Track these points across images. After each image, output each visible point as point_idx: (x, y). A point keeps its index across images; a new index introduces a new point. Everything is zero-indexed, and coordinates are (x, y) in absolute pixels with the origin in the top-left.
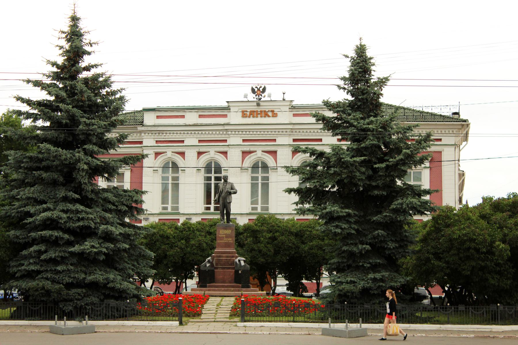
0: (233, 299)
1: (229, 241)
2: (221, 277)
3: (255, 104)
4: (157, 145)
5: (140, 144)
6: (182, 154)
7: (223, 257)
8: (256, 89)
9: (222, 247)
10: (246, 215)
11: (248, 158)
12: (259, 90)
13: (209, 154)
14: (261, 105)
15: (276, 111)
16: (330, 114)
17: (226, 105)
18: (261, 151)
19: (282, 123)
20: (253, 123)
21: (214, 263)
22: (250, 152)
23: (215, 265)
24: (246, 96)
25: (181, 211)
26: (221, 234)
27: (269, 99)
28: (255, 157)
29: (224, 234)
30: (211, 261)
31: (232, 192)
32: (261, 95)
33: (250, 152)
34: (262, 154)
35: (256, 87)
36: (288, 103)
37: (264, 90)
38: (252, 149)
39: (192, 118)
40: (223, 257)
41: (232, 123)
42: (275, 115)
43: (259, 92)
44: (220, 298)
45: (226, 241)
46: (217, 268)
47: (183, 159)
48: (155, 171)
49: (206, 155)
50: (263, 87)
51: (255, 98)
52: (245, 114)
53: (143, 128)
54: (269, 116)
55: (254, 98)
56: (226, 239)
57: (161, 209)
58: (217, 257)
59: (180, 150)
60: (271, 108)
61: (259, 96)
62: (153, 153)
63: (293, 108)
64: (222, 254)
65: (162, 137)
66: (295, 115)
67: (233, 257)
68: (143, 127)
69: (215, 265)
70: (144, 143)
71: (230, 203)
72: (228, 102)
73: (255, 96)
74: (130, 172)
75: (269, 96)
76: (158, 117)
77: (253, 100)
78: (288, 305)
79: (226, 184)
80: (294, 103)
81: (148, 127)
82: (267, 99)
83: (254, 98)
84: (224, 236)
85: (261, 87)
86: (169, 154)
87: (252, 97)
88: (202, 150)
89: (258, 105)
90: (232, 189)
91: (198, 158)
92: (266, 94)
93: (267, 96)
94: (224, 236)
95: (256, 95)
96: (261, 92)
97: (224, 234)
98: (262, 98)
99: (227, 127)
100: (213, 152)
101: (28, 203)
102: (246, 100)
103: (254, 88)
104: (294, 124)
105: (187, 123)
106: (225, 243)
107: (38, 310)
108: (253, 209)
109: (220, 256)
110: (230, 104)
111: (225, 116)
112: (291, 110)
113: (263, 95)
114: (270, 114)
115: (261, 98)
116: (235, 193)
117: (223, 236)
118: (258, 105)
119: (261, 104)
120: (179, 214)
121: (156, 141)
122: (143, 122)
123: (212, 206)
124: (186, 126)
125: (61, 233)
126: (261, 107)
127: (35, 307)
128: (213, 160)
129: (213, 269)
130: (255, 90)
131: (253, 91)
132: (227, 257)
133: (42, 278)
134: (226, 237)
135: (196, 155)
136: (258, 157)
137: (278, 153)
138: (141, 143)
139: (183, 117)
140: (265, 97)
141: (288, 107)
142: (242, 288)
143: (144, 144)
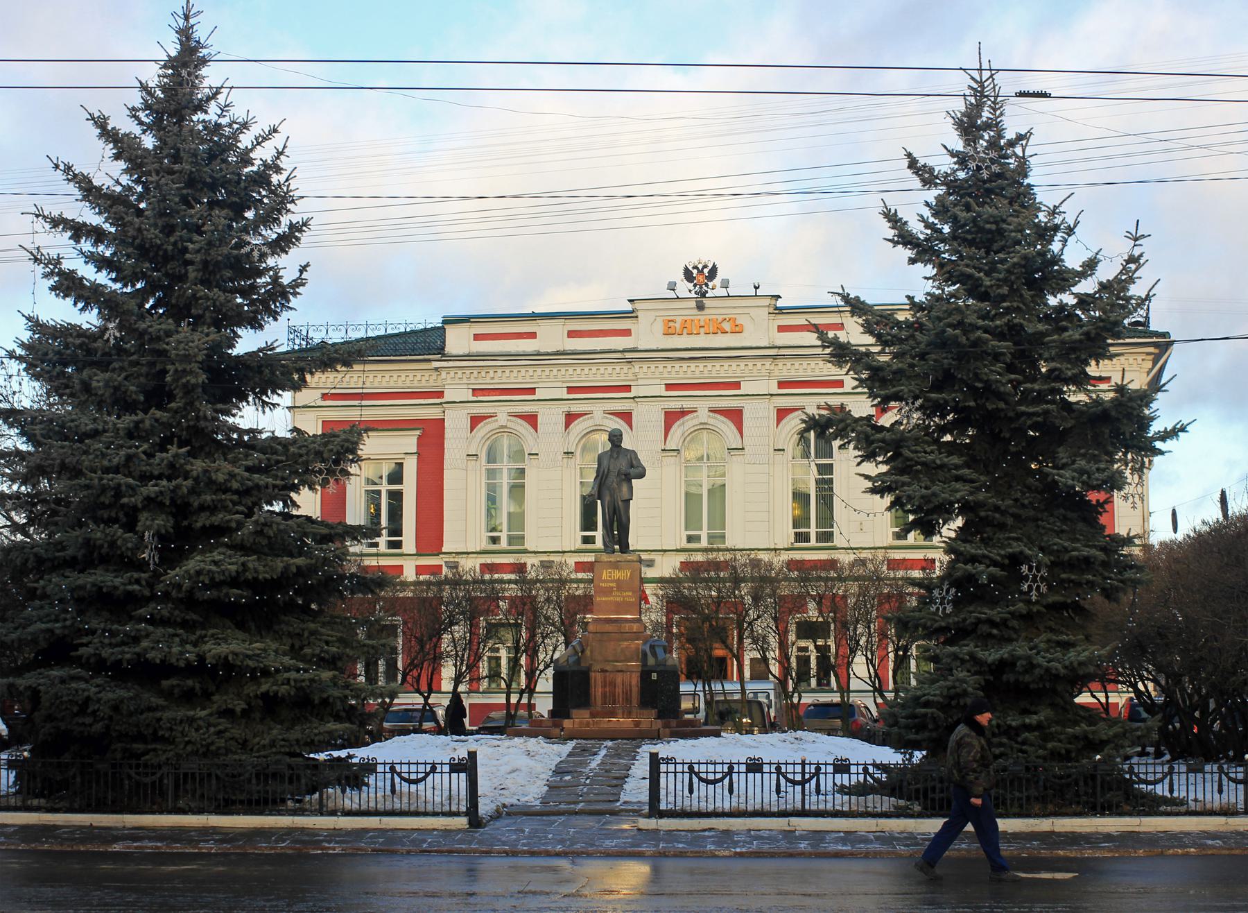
1: (627, 599)
3: (693, 304)
4: (475, 399)
6: (532, 420)
8: (695, 272)
11: (679, 426)
12: (701, 272)
13: (592, 418)
16: (854, 334)
17: (629, 307)
19: (754, 345)
22: (683, 413)
24: (672, 287)
25: (529, 545)
26: (605, 581)
27: (723, 292)
28: (695, 422)
29: (612, 581)
31: (632, 474)
32: (707, 285)
33: (683, 413)
34: (709, 416)
35: (696, 267)
37: (713, 272)
38: (687, 404)
39: (552, 337)
41: (641, 348)
42: (738, 330)
43: (700, 278)
45: (618, 599)
47: (532, 430)
48: (471, 458)
50: (710, 266)
55: (690, 291)
56: (618, 594)
59: (527, 409)
61: (701, 287)
63: (780, 311)
65: (487, 381)
66: (782, 329)
70: (446, 394)
71: (627, 502)
72: (630, 301)
73: (692, 288)
74: (415, 461)
75: (725, 284)
76: (477, 337)
77: (690, 295)
79: (618, 453)
80: (780, 303)
82: (721, 292)
83: (690, 291)
85: (705, 267)
86: (502, 419)
87: (684, 288)
88: (576, 408)
89: (700, 307)
90: (632, 466)
92: (717, 281)
93: (718, 285)
94: (614, 585)
95: (695, 286)
97: (612, 581)
99: (628, 355)
101: (1068, 751)
102: (671, 295)
103: (690, 268)
105: (542, 350)
107: (154, 783)
108: (690, 539)
110: (638, 306)
111: (626, 333)
113: (711, 284)
114: (727, 326)
115: (707, 292)
116: (642, 475)
117: (611, 585)
118: (700, 307)
119: (707, 302)
120: (525, 552)
122: (443, 349)
123: (599, 534)
126: (706, 311)
127: (146, 775)
131: (688, 275)
133: (541, 672)
136: (701, 424)
137: (746, 415)
138: (440, 394)
139: (532, 335)
140: (716, 289)
143: (447, 397)
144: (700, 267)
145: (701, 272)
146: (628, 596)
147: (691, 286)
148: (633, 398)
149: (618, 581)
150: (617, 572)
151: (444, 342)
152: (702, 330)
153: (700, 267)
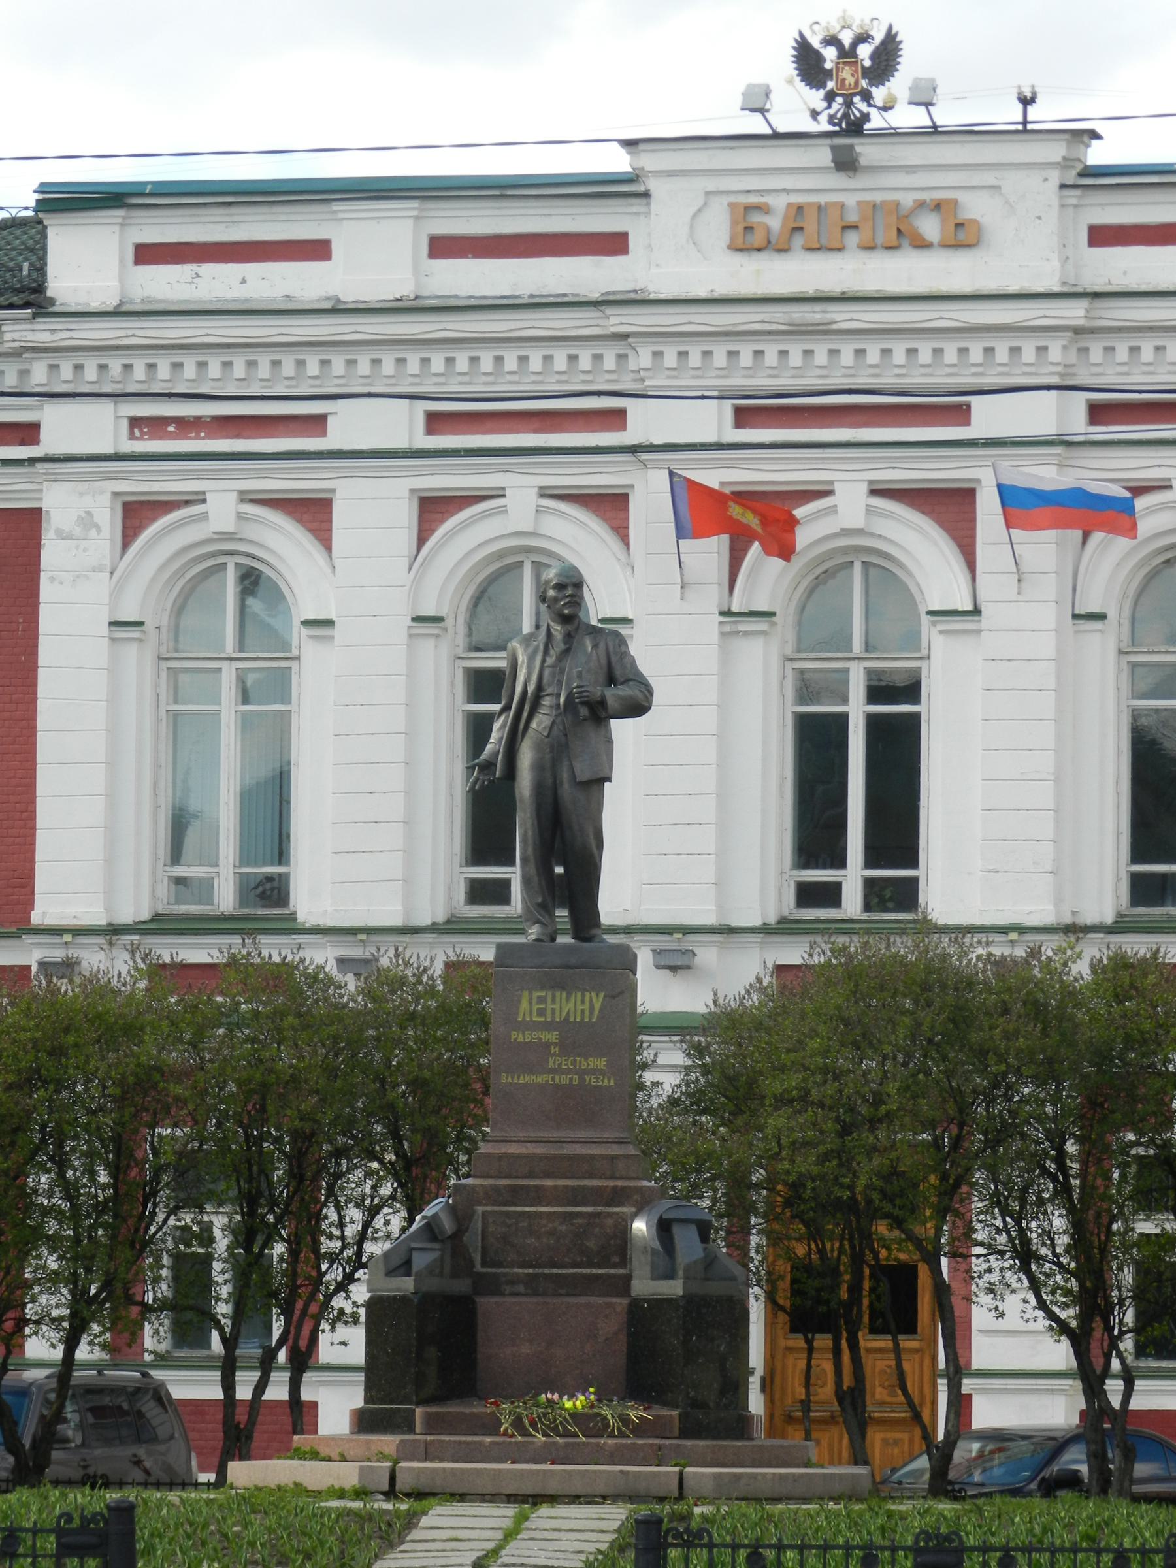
0: (614, 1516)
1: (590, 1080)
2: (525, 1349)
3: (823, 155)
5: (23, 443)
7: (539, 1195)
8: (830, 54)
9: (606, 1178)
10: (757, 938)
12: (847, 54)
14: (863, 161)
15: (975, 207)
17: (619, 162)
18: (864, 488)
20: (810, 289)
21: (473, 1241)
23: (477, 1258)
24: (757, 104)
27: (916, 118)
29: (548, 1026)
30: (448, 1226)
32: (867, 97)
35: (832, 41)
36: (1056, 151)
40: (539, 1195)
43: (847, 74)
44: (510, 1511)
45: (564, 1080)
46: (489, 1286)
48: (122, 633)
49: (473, 520)
50: (879, 36)
51: (823, 118)
52: (749, 229)
53: (42, 332)
54: (921, 244)
55: (815, 114)
56: (565, 1062)
57: (163, 890)
58: (493, 1194)
60: (939, 184)
61: (849, 104)
62: (106, 499)
64: (531, 1175)
66: (1101, 236)
67: (617, 1197)
68: (43, 324)
69: (477, 1258)
72: (630, 144)
73: (820, 105)
76: (146, 254)
78: (780, 1548)
80: (1097, 155)
81: (73, 323)
82: (908, 117)
84: (552, 1037)
85: (862, 38)
90: (611, 680)
91: (422, 541)
92: (898, 85)
94: (552, 1037)
95: (830, 97)
96: (866, 72)
97: (548, 1026)
98: (873, 112)
99: (618, 320)
100: (531, 498)
103: (815, 42)
104: (1096, 295)
105: (350, 295)
106: (557, 1087)
109: (516, 1195)
110: (650, 161)
111: (615, 244)
112: (1073, 196)
113: (879, 94)
114: (930, 226)
116: (637, 708)
117: (546, 1036)
119: (866, 151)
121: (135, 422)
124: (338, 309)
125: (225, 1291)
128: (528, 550)
129: (462, 1286)
130: (819, 58)
132: (576, 1196)
134: (566, 1048)
135: (406, 515)
136: (846, 532)
139: (318, 250)
141: (1055, 178)
142: (684, 1434)
143: (49, 443)
144: (847, 38)
145: (847, 54)
146: (595, 1072)
147: (816, 98)
148: (633, 450)
149: (564, 1027)
150: (561, 995)
151: (40, 269)
152: (852, 238)
153: (847, 38)
